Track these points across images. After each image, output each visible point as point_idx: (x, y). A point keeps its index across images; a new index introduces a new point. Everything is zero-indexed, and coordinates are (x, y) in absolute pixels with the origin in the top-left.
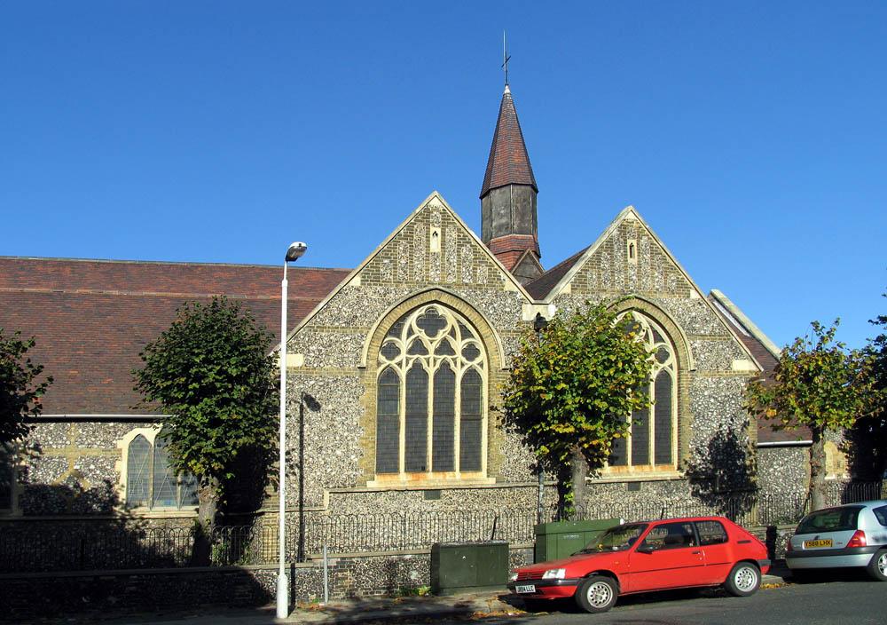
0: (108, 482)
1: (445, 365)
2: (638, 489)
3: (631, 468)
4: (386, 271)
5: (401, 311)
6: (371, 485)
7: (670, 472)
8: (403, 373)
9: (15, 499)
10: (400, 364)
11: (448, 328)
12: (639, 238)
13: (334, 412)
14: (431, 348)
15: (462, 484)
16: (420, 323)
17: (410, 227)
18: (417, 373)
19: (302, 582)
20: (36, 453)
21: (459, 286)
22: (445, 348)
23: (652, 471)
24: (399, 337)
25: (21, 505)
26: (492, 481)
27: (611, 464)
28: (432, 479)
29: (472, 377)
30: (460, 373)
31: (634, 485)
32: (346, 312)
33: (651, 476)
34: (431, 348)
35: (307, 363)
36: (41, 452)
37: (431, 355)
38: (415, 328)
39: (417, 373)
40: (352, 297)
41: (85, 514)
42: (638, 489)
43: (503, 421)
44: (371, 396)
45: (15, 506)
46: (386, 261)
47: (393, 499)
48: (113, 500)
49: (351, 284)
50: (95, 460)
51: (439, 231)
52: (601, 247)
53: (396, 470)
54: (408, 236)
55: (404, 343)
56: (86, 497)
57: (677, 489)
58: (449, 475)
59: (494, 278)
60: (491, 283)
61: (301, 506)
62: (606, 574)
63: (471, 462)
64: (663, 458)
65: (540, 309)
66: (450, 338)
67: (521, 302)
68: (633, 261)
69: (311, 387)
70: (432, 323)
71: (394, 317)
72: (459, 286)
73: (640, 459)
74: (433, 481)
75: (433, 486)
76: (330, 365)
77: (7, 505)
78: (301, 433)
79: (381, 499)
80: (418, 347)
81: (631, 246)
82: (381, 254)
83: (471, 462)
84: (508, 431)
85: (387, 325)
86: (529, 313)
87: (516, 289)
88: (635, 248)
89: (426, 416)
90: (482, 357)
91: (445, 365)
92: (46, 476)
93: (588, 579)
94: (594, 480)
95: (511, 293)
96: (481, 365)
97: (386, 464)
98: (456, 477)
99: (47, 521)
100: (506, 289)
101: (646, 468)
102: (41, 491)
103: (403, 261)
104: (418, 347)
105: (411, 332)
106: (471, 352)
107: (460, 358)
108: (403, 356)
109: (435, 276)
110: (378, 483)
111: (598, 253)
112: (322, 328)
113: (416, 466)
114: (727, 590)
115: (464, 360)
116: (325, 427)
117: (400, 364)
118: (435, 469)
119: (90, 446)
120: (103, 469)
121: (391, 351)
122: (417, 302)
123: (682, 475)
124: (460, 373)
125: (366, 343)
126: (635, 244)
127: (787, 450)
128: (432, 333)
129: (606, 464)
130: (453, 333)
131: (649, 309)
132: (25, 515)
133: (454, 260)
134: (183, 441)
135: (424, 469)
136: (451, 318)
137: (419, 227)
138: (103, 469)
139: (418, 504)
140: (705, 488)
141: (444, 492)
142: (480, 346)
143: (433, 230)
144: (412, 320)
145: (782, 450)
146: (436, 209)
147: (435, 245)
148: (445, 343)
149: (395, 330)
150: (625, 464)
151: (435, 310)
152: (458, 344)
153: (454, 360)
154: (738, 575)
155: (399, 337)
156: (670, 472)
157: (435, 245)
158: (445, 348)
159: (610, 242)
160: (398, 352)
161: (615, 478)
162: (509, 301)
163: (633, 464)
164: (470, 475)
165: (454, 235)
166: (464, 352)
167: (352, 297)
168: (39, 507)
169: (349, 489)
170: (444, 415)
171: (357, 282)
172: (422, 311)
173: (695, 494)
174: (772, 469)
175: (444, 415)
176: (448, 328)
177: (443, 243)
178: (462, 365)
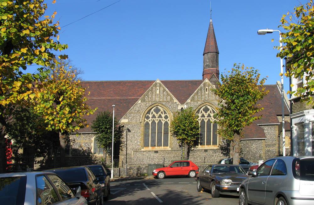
0: (89, 148)
1: (160, 120)
2: (207, 151)
3: (206, 146)
4: (146, 99)
5: (199, 107)
6: (142, 150)
7: (216, 147)
8: (150, 123)
9: (70, 152)
10: (199, 120)
11: (161, 112)
12: (209, 86)
13: (134, 132)
14: (206, 116)
15: (163, 150)
16: (203, 110)
17: (152, 88)
18: (153, 122)
19: (122, 172)
20: (74, 142)
21: (163, 101)
22: (209, 116)
23: (212, 147)
24: (150, 114)
25: (71, 154)
26: (170, 149)
27: (201, 145)
28: (157, 148)
29: (166, 123)
30: (163, 122)
31: (206, 151)
32: (137, 109)
33: (210, 148)
34: (206, 116)
35: (129, 121)
36: (75, 141)
37: (206, 118)
38: (153, 112)
39: (153, 122)
40: (139, 105)
41: (85, 156)
42: (207, 151)
43: (173, 134)
44: (142, 129)
45: (70, 154)
46: (146, 96)
47: (147, 153)
48: (90, 153)
49: (138, 102)
50: (87, 143)
51: (159, 88)
52: (199, 89)
53: (210, 144)
54: (152, 90)
55: (150, 116)
56: (84, 152)
57: (218, 152)
58: (161, 147)
59: (172, 99)
60: (171, 101)
61: (126, 155)
62: (163, 171)
63: (166, 144)
64: (215, 143)
65: (182, 106)
66: (161, 114)
67: (178, 105)
68: (207, 93)
69: (129, 127)
70: (157, 111)
71: (148, 110)
72: (163, 101)
73: (208, 144)
74: (156, 149)
75: (156, 150)
76: (134, 121)
77: (68, 154)
78: (127, 137)
79: (145, 153)
80: (203, 116)
81: (207, 89)
82: (145, 95)
83: (166, 144)
84: (174, 137)
85: (146, 112)
86: (180, 107)
87: (177, 102)
88: (208, 89)
89: (205, 132)
90: (169, 118)
91: (160, 120)
92: (75, 146)
93: (159, 172)
94: (195, 149)
95: (176, 102)
96: (168, 120)
97: (146, 145)
98: (162, 148)
99: (77, 157)
100: (174, 102)
101: (210, 146)
102: (75, 150)
103: (150, 96)
104: (203, 116)
105: (152, 113)
106: (166, 117)
107: (164, 119)
108: (150, 119)
109: (157, 99)
110: (145, 149)
111: (198, 91)
112: (132, 113)
113: (153, 145)
114: (188, 176)
115: (165, 119)
116: (132, 136)
117: (150, 121)
118: (158, 146)
119: (86, 140)
120: (89, 145)
121: (148, 118)
122: (153, 106)
123: (219, 148)
124: (163, 122)
125: (141, 116)
126: (208, 88)
127: (257, 140)
128: (157, 113)
129: (199, 145)
130: (211, 112)
131: (211, 105)
132: (72, 156)
133: (162, 95)
134: (99, 140)
135: (155, 146)
136: (162, 110)
137: (154, 87)
138: (89, 145)
139: (153, 154)
140: (225, 152)
141: (159, 152)
142: (168, 116)
143: (157, 88)
144: (202, 109)
145: (256, 141)
146: (158, 83)
147: (158, 92)
148: (160, 115)
149: (149, 112)
150: (162, 146)
151: (158, 107)
152: (163, 116)
153: (162, 119)
154: (191, 173)
155: (150, 114)
156: (216, 147)
157: (158, 92)
158: (160, 116)
159: (201, 88)
160: (199, 117)
161: (201, 149)
162: (175, 105)
163: (151, 146)
164: (165, 147)
165: (162, 89)
166: (165, 117)
167: (139, 105)
168: (75, 154)
169: (137, 151)
170: (160, 132)
171: (140, 102)
172: (204, 107)
173: (222, 153)
174: (252, 146)
175: (160, 132)
176: (210, 111)
177: (160, 91)
178: (164, 120)
